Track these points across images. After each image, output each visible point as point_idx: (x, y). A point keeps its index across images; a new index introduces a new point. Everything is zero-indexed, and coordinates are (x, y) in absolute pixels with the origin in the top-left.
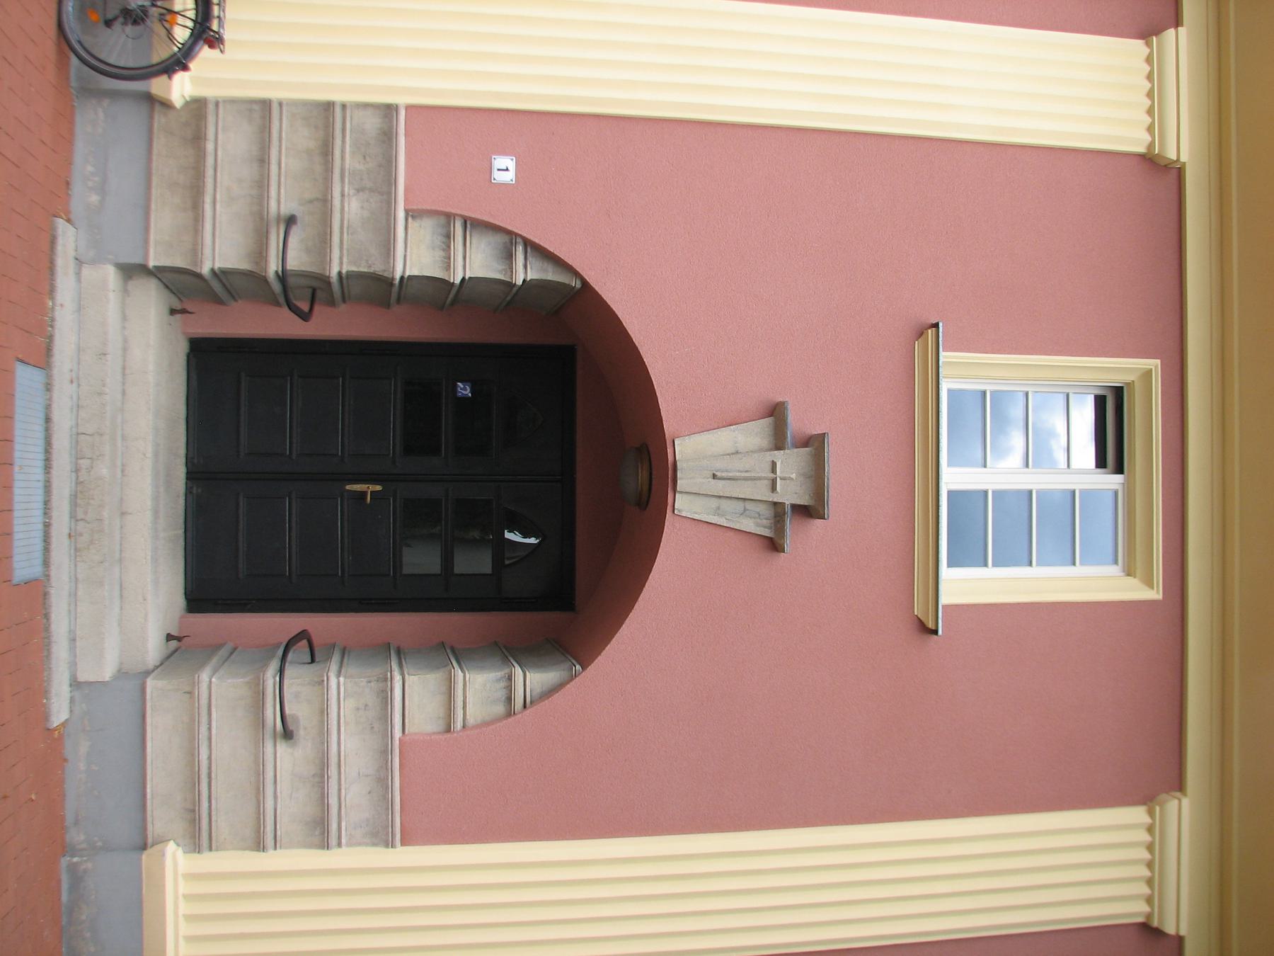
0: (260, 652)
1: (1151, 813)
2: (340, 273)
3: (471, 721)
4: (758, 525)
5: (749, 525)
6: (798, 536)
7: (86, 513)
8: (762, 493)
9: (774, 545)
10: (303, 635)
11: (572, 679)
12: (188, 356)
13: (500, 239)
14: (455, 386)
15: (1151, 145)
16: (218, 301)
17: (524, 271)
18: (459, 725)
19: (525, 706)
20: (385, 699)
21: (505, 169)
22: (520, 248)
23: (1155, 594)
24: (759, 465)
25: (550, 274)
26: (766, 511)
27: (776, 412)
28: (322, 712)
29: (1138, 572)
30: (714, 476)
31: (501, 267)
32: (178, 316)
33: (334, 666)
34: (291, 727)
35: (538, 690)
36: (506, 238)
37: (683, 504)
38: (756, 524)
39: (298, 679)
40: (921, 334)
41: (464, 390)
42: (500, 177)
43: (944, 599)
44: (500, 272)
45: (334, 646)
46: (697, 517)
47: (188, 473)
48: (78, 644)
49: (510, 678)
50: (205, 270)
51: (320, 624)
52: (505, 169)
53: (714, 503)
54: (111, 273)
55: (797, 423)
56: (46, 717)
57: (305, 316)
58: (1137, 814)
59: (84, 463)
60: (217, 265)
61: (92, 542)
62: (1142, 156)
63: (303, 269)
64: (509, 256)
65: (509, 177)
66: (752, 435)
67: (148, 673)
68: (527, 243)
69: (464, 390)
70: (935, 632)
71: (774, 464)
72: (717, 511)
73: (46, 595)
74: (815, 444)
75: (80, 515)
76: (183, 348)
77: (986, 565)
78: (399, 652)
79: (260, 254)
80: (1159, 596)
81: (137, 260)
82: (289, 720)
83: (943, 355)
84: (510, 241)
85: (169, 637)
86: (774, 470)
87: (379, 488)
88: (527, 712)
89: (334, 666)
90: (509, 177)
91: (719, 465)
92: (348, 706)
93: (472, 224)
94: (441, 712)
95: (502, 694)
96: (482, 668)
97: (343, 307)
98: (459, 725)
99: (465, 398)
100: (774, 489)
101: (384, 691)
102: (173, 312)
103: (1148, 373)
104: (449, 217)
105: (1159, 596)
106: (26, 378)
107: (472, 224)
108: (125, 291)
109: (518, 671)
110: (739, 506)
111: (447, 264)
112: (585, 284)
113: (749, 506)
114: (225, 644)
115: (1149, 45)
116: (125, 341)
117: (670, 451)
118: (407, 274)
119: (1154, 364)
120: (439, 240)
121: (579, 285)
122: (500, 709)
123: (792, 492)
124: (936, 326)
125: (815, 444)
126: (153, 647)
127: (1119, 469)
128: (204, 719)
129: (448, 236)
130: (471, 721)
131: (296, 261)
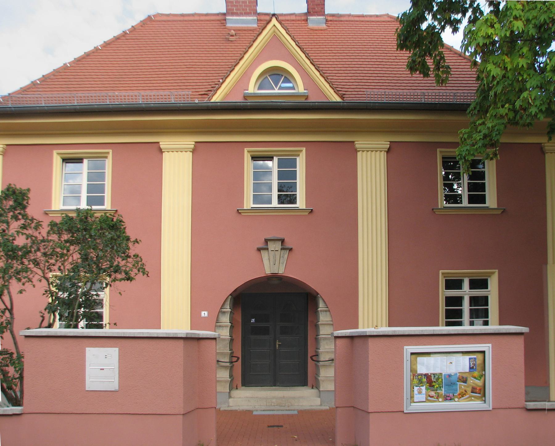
0: (317, 368)
1: (359, 151)
2: (229, 350)
3: (331, 319)
4: (286, 254)
5: (286, 256)
6: (288, 245)
7: (284, 404)
8: (278, 254)
9: (291, 250)
10: (311, 358)
11: (321, 297)
12: (246, 387)
13: (220, 314)
14: (252, 322)
15: (190, 151)
16: (233, 378)
17: (228, 309)
18: (331, 322)
19: (327, 307)
20: (325, 339)
21: (204, 314)
22: (222, 310)
23: (304, 149)
24: (272, 254)
25: (228, 302)
26: (283, 251)
27: (259, 250)
28: (328, 353)
29: (299, 153)
30: (275, 264)
31: (227, 314)
32: (238, 388)
33: (319, 351)
34: (331, 359)
35: (324, 304)
36: (220, 313)
37: (281, 271)
38: (286, 254)
39: (322, 358)
40: (240, 213)
41: (253, 320)
42: (203, 313)
43: (304, 208)
44: (228, 314)
45: (315, 351)
46: (284, 268)
47: (274, 386)
48: (312, 405)
49: (321, 311)
50: (230, 379)
51: (310, 353)
52: (204, 314)
53: (281, 264)
54: (230, 400)
55: (261, 245)
56: (327, 410)
57: (238, 358)
58: (359, 154)
59: (273, 404)
60: (229, 377)
61: (290, 402)
62: (193, 153)
63: (229, 357)
64: (224, 312)
65: (206, 313)
66: (264, 254)
67: (319, 391)
68: (221, 308)
69: (253, 320)
70: (312, 210)
71: (272, 251)
72: (283, 263)
73: (301, 410)
74: (267, 241)
75: (284, 405)
76: (243, 387)
77: (296, 182)
78: (317, 336)
79: (226, 367)
80: (305, 148)
81: (228, 394)
82: (330, 360)
83: (245, 208)
84: (221, 312)
85: (312, 388)
86: (273, 251)
87: (277, 341)
88: (329, 307)
89: (319, 351)
90: (206, 313)
91: (272, 263)
92: (327, 347)
93: (217, 321)
94: (328, 326)
95: (325, 313)
96: (319, 317)
97: (234, 350)
98: (331, 322)
99: (255, 320)
100: (277, 250)
101: (323, 339)
102: (237, 389)
103: (248, 151)
104: (216, 326)
105: (305, 148)
106: (255, 413)
107: (217, 321)
108: (234, 398)
109: (319, 309)
110: (281, 258)
111: (226, 326)
112: (230, 295)
113: (281, 256)
114: (315, 377)
115: (164, 152)
116: (245, 397)
117: (269, 275)
118: (229, 335)
119: (246, 150)
120: (221, 328)
121: (230, 296)
122: (328, 313)
123: (278, 246)
124: (238, 210)
125: (267, 241)
126: (315, 391)
127: (273, 158)
128: (329, 378)
129: (220, 326)
130: (331, 319)
131: (227, 360)
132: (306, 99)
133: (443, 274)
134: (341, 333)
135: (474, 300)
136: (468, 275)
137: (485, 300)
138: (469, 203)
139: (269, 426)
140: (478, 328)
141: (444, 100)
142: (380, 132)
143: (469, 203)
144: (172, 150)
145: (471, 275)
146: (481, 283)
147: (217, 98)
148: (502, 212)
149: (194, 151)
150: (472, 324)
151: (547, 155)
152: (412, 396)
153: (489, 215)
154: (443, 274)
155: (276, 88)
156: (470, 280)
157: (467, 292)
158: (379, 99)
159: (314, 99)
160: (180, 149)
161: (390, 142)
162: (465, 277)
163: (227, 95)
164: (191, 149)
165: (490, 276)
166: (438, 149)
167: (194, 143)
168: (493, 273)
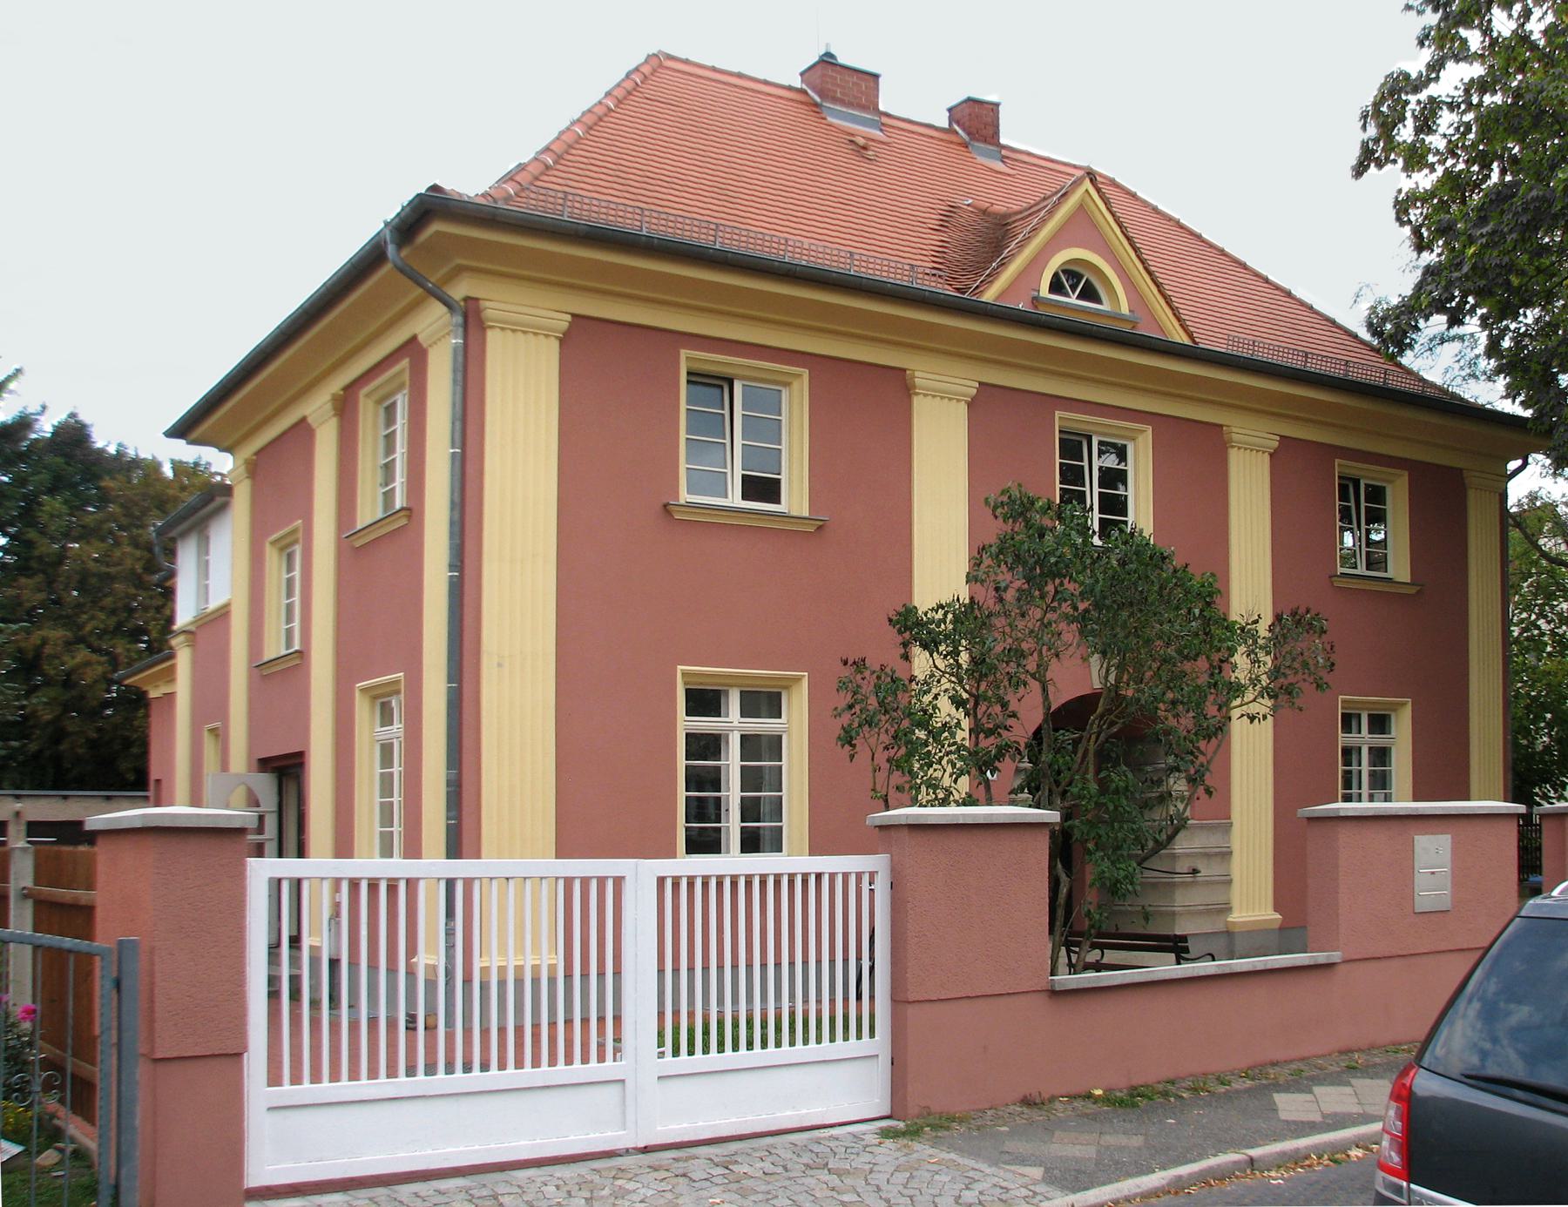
43: (806, 513)
132: (1133, 328)
133: (684, 674)
134: (907, 816)
135: (751, 744)
136: (1367, 706)
137: (773, 745)
138: (745, 497)
139: (269, 1109)
140: (1380, 806)
141: (871, 272)
142: (1273, 414)
143: (745, 497)
144: (515, 328)
145: (1372, 706)
146: (1380, 723)
147: (989, 296)
148: (1418, 592)
149: (565, 341)
150: (1371, 798)
151: (490, 334)
152: (430, 1021)
153: (788, 532)
154: (684, 674)
155: (1073, 293)
156: (1369, 715)
157: (736, 724)
158: (834, 264)
159: (1144, 330)
160: (523, 326)
161: (980, 383)
162: (1363, 709)
163: (1003, 294)
164: (559, 333)
165: (787, 688)
166: (1057, 412)
167: (569, 318)
168: (1404, 704)
